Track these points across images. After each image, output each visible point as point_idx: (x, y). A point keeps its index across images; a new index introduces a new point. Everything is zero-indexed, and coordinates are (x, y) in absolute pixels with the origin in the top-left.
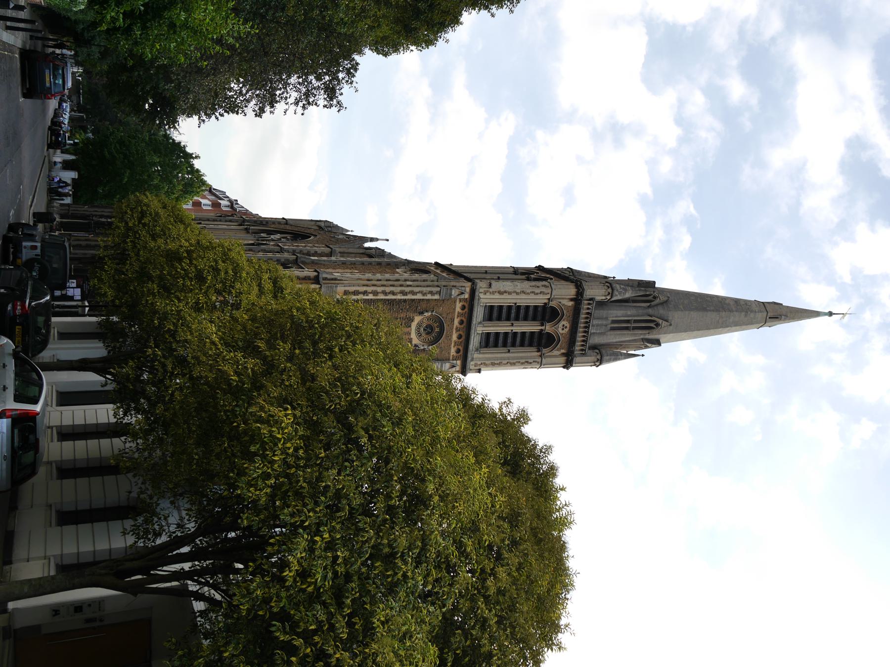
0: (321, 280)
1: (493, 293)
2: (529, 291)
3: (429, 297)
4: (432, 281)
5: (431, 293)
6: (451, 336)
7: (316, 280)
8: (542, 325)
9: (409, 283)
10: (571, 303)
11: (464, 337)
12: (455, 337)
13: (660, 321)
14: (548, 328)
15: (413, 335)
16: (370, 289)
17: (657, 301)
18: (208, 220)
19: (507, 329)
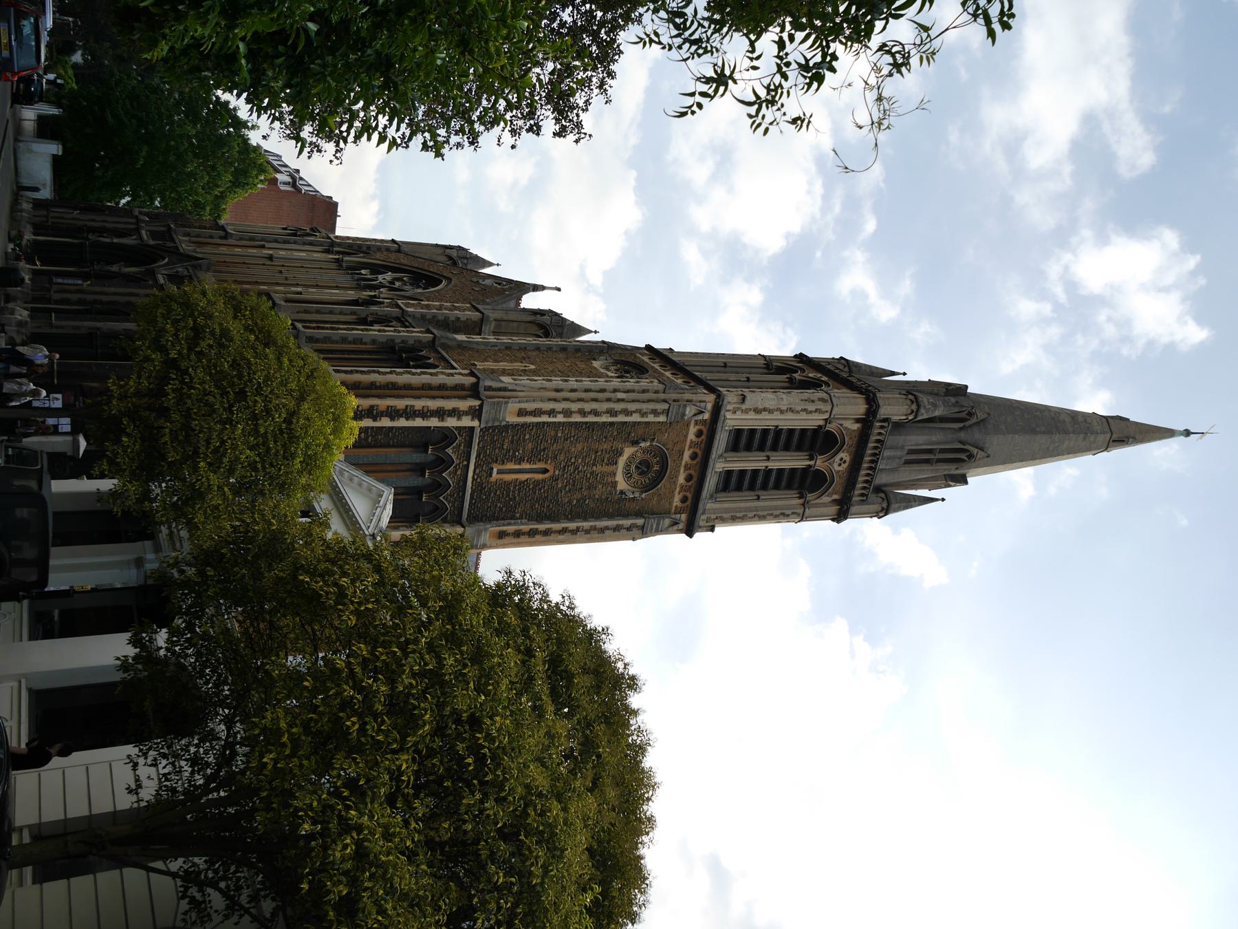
0: (481, 389)
1: (746, 411)
2: (799, 408)
3: (651, 418)
4: (656, 392)
6: (677, 477)
7: (474, 392)
8: (811, 458)
9: (620, 395)
10: (856, 426)
11: (695, 479)
12: (681, 479)
13: (975, 451)
14: (820, 463)
15: (619, 478)
16: (559, 406)
17: (974, 420)
18: (276, 241)
19: (761, 465)
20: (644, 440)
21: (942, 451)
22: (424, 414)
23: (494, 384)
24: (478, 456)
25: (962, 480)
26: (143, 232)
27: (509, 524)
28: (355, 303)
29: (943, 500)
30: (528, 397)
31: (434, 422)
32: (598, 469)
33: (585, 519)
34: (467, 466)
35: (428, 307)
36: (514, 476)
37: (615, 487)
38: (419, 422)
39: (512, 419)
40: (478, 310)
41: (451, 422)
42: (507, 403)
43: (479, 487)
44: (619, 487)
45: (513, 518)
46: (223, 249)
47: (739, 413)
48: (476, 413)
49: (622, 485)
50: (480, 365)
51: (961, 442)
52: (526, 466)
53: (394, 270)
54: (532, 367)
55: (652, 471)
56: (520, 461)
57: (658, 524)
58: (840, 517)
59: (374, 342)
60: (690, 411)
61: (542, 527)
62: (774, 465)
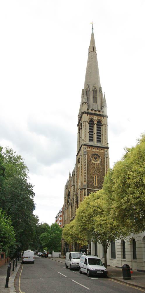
3: (86, 158)
5: (85, 157)
7: (81, 189)
8: (95, 124)
10: (88, 115)
12: (98, 151)
14: (95, 123)
15: (97, 163)
21: (94, 95)
24: (92, 188)
32: (95, 167)
34: (94, 190)
36: (96, 182)
39: (86, 183)
44: (99, 162)
47: (86, 141)
48: (85, 189)
52: (95, 180)
53: (68, 199)
55: (96, 156)
56: (94, 181)
59: (76, 205)
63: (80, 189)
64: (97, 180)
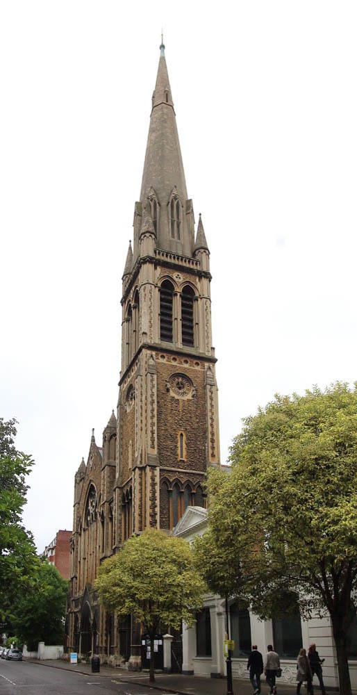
0: (141, 466)
3: (155, 382)
5: (152, 381)
10: (159, 269)
11: (187, 359)
12: (186, 366)
14: (179, 289)
18: (77, 557)
19: (180, 323)
20: (166, 386)
22: (154, 492)
23: (139, 460)
25: (189, 203)
26: (75, 611)
27: (208, 452)
28: (103, 523)
29: (200, 214)
30: (143, 444)
31: (157, 488)
33: (206, 415)
35: (103, 491)
37: (190, 400)
38: (158, 494)
39: (155, 452)
40: (104, 468)
41: (157, 480)
42: (148, 454)
43: (190, 466)
45: (205, 450)
46: (81, 578)
48: (153, 468)
49: (189, 396)
50: (130, 466)
51: (167, 205)
53: (87, 506)
54: (131, 442)
55: (182, 380)
56: (176, 447)
57: (210, 378)
58: (207, 276)
60: (151, 362)
61: (210, 436)
62: (180, 317)
63: (140, 469)
64: (184, 445)
